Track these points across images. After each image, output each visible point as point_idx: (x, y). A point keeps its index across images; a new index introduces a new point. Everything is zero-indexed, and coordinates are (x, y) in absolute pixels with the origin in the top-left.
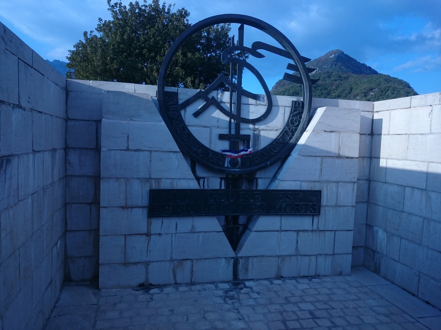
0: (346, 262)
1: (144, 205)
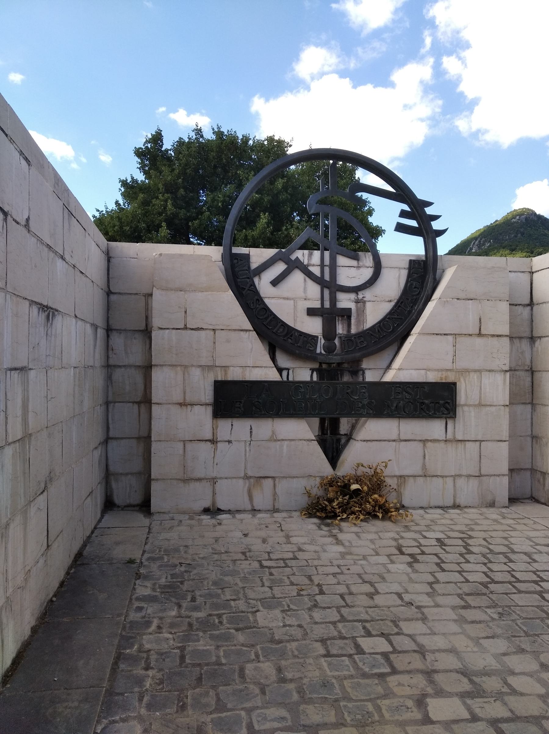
0: (501, 488)
1: (207, 401)
